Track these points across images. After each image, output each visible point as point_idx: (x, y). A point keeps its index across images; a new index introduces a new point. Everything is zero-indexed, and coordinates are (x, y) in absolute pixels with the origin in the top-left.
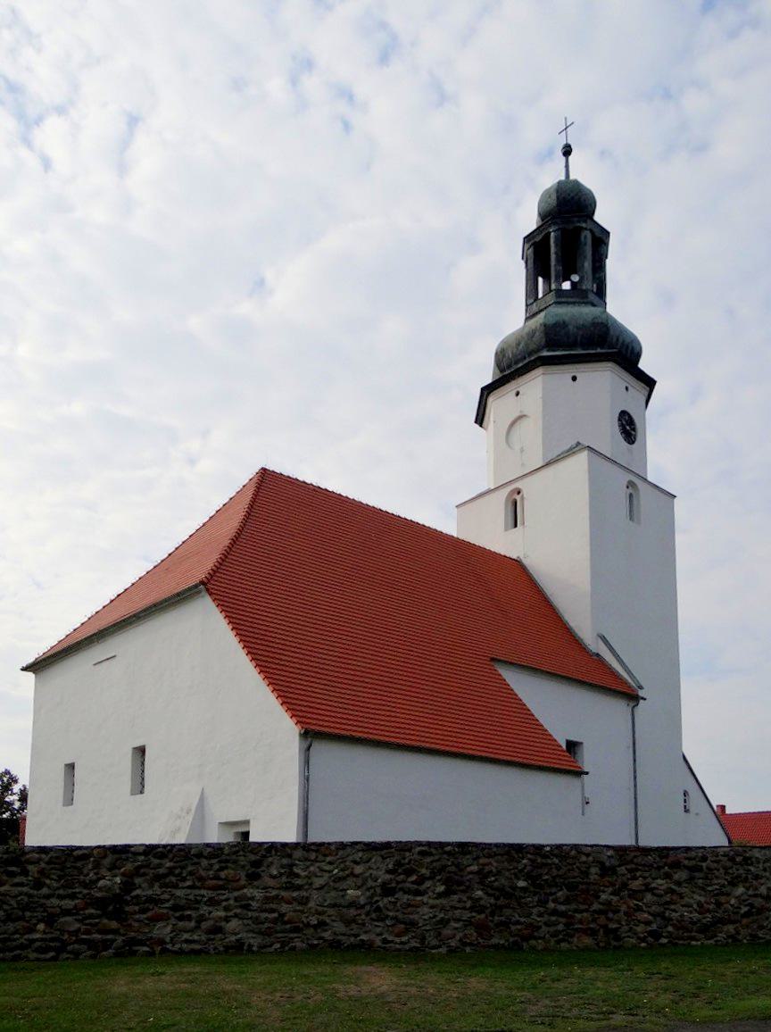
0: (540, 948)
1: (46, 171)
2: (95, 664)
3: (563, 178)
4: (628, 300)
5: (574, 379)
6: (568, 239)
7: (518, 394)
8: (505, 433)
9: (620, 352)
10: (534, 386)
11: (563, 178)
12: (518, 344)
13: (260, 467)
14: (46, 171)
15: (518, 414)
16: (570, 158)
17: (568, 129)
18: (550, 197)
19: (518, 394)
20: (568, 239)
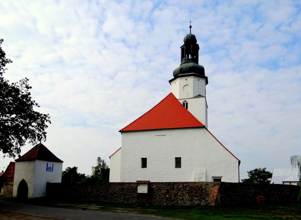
0: (181, 189)
1: (120, 131)
2: (156, 136)
3: (189, 33)
4: (203, 60)
5: (186, 80)
6: (190, 47)
7: (175, 83)
8: (182, 89)
9: (199, 73)
10: (178, 81)
11: (189, 33)
12: (186, 69)
13: (31, 94)
14: (120, 131)
15: (186, 84)
16: (191, 28)
17: (191, 22)
18: (190, 37)
19: (175, 83)
20: (190, 47)
